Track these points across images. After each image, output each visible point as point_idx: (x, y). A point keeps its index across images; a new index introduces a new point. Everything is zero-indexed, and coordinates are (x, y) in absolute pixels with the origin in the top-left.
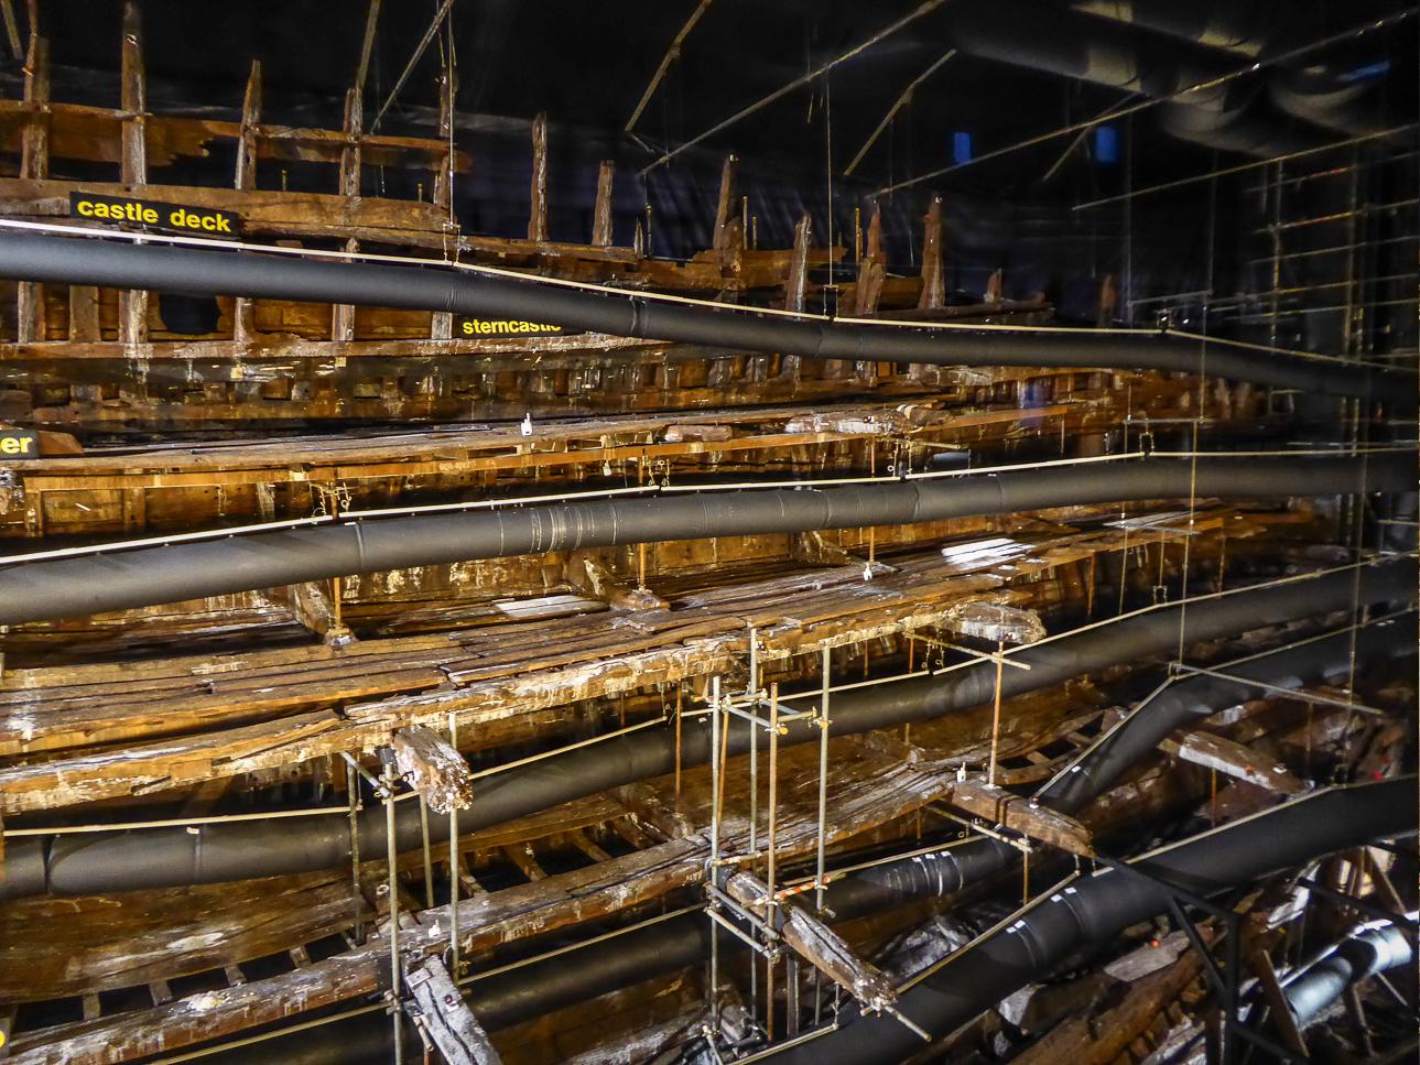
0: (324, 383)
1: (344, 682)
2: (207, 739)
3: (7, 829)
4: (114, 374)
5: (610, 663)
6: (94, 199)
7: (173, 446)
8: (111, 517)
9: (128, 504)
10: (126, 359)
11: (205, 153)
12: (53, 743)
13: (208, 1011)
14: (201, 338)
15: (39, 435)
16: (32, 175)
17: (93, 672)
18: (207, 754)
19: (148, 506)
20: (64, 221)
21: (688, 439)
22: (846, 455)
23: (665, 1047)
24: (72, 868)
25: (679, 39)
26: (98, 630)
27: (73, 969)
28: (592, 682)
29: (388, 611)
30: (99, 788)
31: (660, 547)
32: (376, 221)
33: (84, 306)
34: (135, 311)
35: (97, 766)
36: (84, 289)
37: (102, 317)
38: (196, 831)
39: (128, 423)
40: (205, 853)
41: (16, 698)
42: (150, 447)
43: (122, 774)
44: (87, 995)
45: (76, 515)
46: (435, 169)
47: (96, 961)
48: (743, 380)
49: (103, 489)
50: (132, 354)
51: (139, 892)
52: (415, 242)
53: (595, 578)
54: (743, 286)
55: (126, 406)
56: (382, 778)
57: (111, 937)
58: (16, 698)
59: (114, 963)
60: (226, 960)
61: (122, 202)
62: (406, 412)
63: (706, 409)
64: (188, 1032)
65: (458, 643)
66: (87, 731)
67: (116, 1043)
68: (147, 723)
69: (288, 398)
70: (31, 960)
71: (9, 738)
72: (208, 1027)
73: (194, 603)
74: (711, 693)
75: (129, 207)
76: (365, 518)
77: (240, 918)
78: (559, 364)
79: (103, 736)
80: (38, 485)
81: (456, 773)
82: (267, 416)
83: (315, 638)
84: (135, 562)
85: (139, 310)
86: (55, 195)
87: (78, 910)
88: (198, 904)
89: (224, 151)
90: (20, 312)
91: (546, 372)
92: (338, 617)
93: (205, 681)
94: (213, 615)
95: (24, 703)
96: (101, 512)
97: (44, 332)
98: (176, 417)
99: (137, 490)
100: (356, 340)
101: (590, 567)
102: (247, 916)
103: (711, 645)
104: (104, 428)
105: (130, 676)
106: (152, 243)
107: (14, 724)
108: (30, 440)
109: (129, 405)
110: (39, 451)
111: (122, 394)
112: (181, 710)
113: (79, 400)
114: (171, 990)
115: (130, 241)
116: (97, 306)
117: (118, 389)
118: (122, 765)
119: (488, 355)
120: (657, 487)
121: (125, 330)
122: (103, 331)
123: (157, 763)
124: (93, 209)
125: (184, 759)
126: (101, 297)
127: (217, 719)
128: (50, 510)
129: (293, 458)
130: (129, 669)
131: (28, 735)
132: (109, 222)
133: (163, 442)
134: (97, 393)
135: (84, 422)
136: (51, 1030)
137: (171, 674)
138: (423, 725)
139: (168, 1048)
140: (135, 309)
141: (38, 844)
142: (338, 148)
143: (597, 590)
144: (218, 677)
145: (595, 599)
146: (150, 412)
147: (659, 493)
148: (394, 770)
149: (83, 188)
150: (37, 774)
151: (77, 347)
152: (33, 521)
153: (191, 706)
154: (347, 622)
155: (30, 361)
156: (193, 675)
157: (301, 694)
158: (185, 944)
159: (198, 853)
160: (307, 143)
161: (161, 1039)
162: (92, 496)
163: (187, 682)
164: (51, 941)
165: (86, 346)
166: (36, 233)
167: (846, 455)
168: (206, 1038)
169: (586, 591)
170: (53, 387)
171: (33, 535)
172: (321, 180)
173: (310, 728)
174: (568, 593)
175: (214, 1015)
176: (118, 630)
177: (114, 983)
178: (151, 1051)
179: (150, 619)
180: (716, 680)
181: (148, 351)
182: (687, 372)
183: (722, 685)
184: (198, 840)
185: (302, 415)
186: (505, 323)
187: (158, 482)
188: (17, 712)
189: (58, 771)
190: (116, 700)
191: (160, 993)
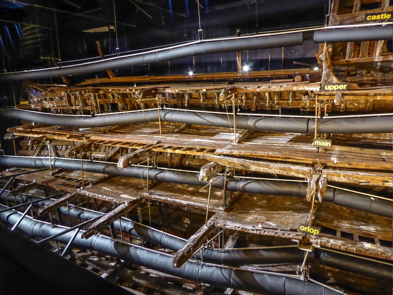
2: (382, 174)
3: (328, 184)
6: (372, 15)
7: (385, 87)
8: (363, 107)
9: (368, 104)
10: (374, 62)
12: (341, 165)
13: (368, 248)
15: (349, 84)
16: (355, 11)
17: (353, 149)
18: (382, 178)
19: (374, 105)
20: (363, 22)
22: (255, 108)
24: (340, 198)
26: (354, 138)
27: (335, 223)
30: (350, 180)
33: (364, 47)
34: (379, 46)
35: (351, 174)
36: (365, 42)
37: (369, 50)
38: (374, 199)
39: (372, 80)
40: (375, 206)
41: (333, 152)
42: (378, 87)
43: (357, 178)
44: (338, 231)
45: (354, 106)
47: (341, 223)
49: (362, 99)
50: (376, 60)
51: (354, 210)
55: (372, 75)
57: (346, 219)
58: (333, 152)
59: (345, 225)
60: (375, 237)
61: (380, 14)
64: (362, 251)
66: (350, 164)
67: (344, 245)
68: (366, 166)
70: (326, 217)
71: (331, 162)
72: (368, 253)
73: (383, 134)
75: (382, 15)
77: (382, 227)
79: (353, 166)
80: (347, 98)
84: (369, 120)
85: (380, 46)
86: (361, 16)
87: (338, 209)
88: (370, 218)
90: (347, 51)
93: (384, 157)
94: (388, 138)
95: (335, 154)
96: (360, 106)
97: (353, 55)
98: (386, 78)
99: (371, 100)
102: (384, 227)
104: (365, 82)
106: (388, 25)
107: (332, 159)
108: (346, 85)
109: (373, 75)
110: (348, 89)
111: (372, 72)
113: (359, 74)
114: (359, 238)
115: (381, 25)
116: (368, 47)
117: (370, 71)
118: (358, 175)
121: (375, 53)
122: (369, 54)
123: (367, 177)
125: (375, 178)
126: (370, 44)
127: (386, 169)
128: (347, 104)
130: (362, 150)
131: (335, 162)
132: (375, 21)
133: (381, 86)
134: (364, 72)
135: (360, 80)
136: (329, 235)
137: (374, 154)
139: (356, 253)
140: (379, 46)
141: (333, 190)
144: (387, 157)
146: (379, 77)
149: (369, 12)
150: (336, 173)
151: (361, 59)
152: (343, 107)
153: (379, 164)
155: (348, 64)
156: (380, 155)
158: (364, 228)
159: (373, 205)
161: (355, 249)
162: (359, 101)
163: (378, 157)
164: (332, 214)
165: (363, 58)
166: (355, 28)
167: (255, 108)
168: (367, 255)
170: (353, 71)
171: (342, 111)
175: (370, 250)
176: (360, 139)
177: (344, 230)
178: (352, 251)
179: (369, 137)
181: (381, 59)
184: (374, 201)
187: (379, 98)
188: (333, 156)
189: (341, 173)
190: (358, 158)
191: (356, 237)
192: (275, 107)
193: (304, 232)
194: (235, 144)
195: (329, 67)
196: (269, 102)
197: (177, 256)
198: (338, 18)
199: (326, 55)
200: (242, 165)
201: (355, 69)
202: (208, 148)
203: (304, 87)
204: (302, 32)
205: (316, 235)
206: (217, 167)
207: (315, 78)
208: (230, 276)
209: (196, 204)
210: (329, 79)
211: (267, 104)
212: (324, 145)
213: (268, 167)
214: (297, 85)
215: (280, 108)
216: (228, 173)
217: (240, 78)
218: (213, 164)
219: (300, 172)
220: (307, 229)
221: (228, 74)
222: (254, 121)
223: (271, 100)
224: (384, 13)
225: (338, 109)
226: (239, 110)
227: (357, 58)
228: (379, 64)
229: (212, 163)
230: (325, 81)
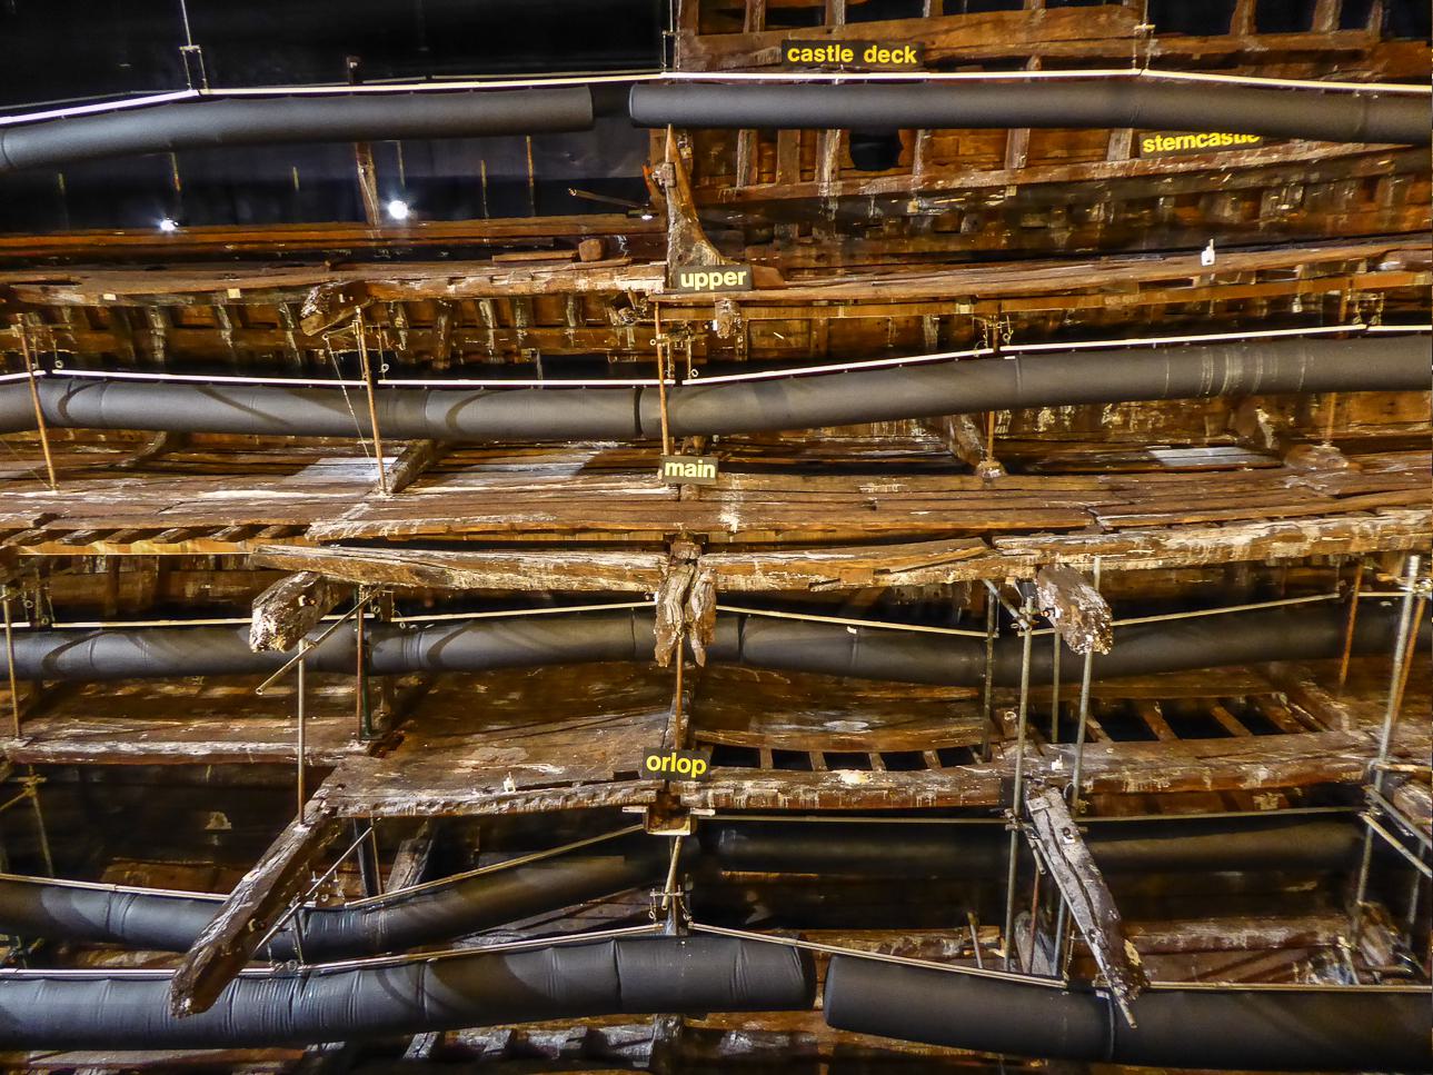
0: (992, 214)
5: (1280, 525)
6: (801, 45)
14: (883, 173)
16: (752, 29)
23: (1288, 945)
28: (1256, 544)
32: (1058, 33)
52: (1099, 53)
53: (1268, 431)
61: (824, 45)
62: (1072, 243)
76: (1025, 352)
78: (1252, 181)
81: (1098, 617)
83: (965, 468)
91: (1234, 191)
92: (989, 451)
101: (1263, 417)
108: (745, 273)
111: (815, 231)
120: (1363, 327)
122: (802, 171)
124: (800, 55)
134: (794, 230)
138: (1066, 564)
143: (1269, 444)
148: (1035, 604)
185: (969, 248)
186: (681, 466)
193: (660, 774)
194: (382, 496)
195: (685, 212)
197: (189, 969)
198: (699, 45)
199: (674, 168)
200: (419, 573)
203: (611, 278)
205: (698, 778)
208: (419, 988)
209: (250, 746)
210: (689, 250)
211: (491, 343)
212: (694, 475)
213: (514, 567)
214: (587, 272)
220: (669, 764)
224: (833, 44)
226: (385, 368)
228: (834, 206)
230: (680, 258)
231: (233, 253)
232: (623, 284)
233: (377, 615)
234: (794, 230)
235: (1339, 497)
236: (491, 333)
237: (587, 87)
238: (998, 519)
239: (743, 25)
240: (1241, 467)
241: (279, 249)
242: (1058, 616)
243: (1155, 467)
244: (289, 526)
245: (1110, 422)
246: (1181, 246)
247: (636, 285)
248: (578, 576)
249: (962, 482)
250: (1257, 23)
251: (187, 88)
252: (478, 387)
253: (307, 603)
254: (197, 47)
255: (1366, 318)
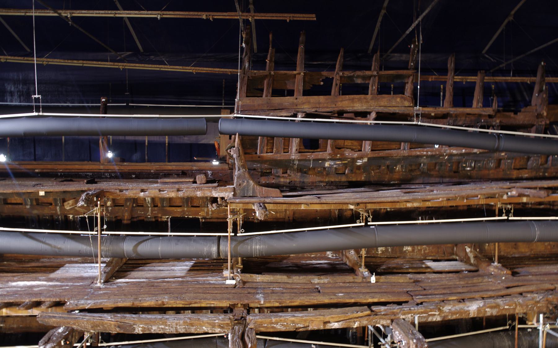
0: (359, 167)
1: (371, 295)
4: (286, 165)
11: (322, 83)
14: (315, 151)
18: (322, 318)
19: (294, 214)
21: (521, 195)
25: (513, 12)
28: (479, 309)
29: (378, 261)
31: (500, 244)
32: (382, 104)
34: (295, 144)
46: (406, 81)
48: (546, 166)
52: (397, 111)
53: (471, 256)
54: (548, 122)
56: (386, 339)
63: (527, 179)
65: (412, 281)
69: (344, 174)
74: (538, 321)
76: (378, 225)
82: (337, 180)
83: (352, 271)
89: (329, 82)
92: (363, 264)
93: (317, 286)
100: (372, 150)
101: (468, 250)
103: (538, 297)
105: (290, 281)
111: (288, 171)
112: (312, 299)
119: (424, 156)
120: (506, 218)
122: (284, 149)
129: (348, 199)
134: (280, 171)
138: (404, 319)
142: (369, 77)
143: (472, 261)
145: (471, 265)
147: (507, 220)
148: (392, 337)
151: (276, 156)
153: (315, 298)
154: (367, 266)
157: (355, 298)
160: (358, 77)
165: (279, 155)
169: (466, 260)
172: (362, 90)
173: (360, 314)
174: (456, 260)
180: (541, 316)
182: (517, 162)
183: (544, 318)
192: (161, 218)
194: (99, 285)
195: (243, 166)
196: (152, 211)
199: (239, 150)
201: (269, 167)
202: (48, 299)
204: (205, 118)
206: (70, 337)
207: (221, 179)
211: (149, 213)
214: (198, 189)
215: (169, 220)
216: (87, 341)
217: (104, 173)
218: (63, 332)
219: (216, 324)
221: (82, 165)
222: (135, 243)
223: (155, 206)
225: (250, 220)
226: (105, 227)
227: (271, 154)
228: (297, 162)
229: (60, 330)
230: (240, 185)
231: (38, 173)
232: (215, 194)
233: (91, 344)
234: (280, 171)
235: (508, 288)
236: (150, 209)
237: (204, 119)
238: (373, 298)
239: (263, 94)
240: (463, 271)
241: (60, 172)
242: (404, 344)
243: (429, 270)
244: (56, 302)
245: (407, 250)
246: (431, 182)
247: (222, 195)
248: (193, 326)
249: (354, 279)
250: (453, 104)
251: (33, 112)
252: (148, 235)
253: (65, 343)
254: (40, 96)
255: (507, 215)
